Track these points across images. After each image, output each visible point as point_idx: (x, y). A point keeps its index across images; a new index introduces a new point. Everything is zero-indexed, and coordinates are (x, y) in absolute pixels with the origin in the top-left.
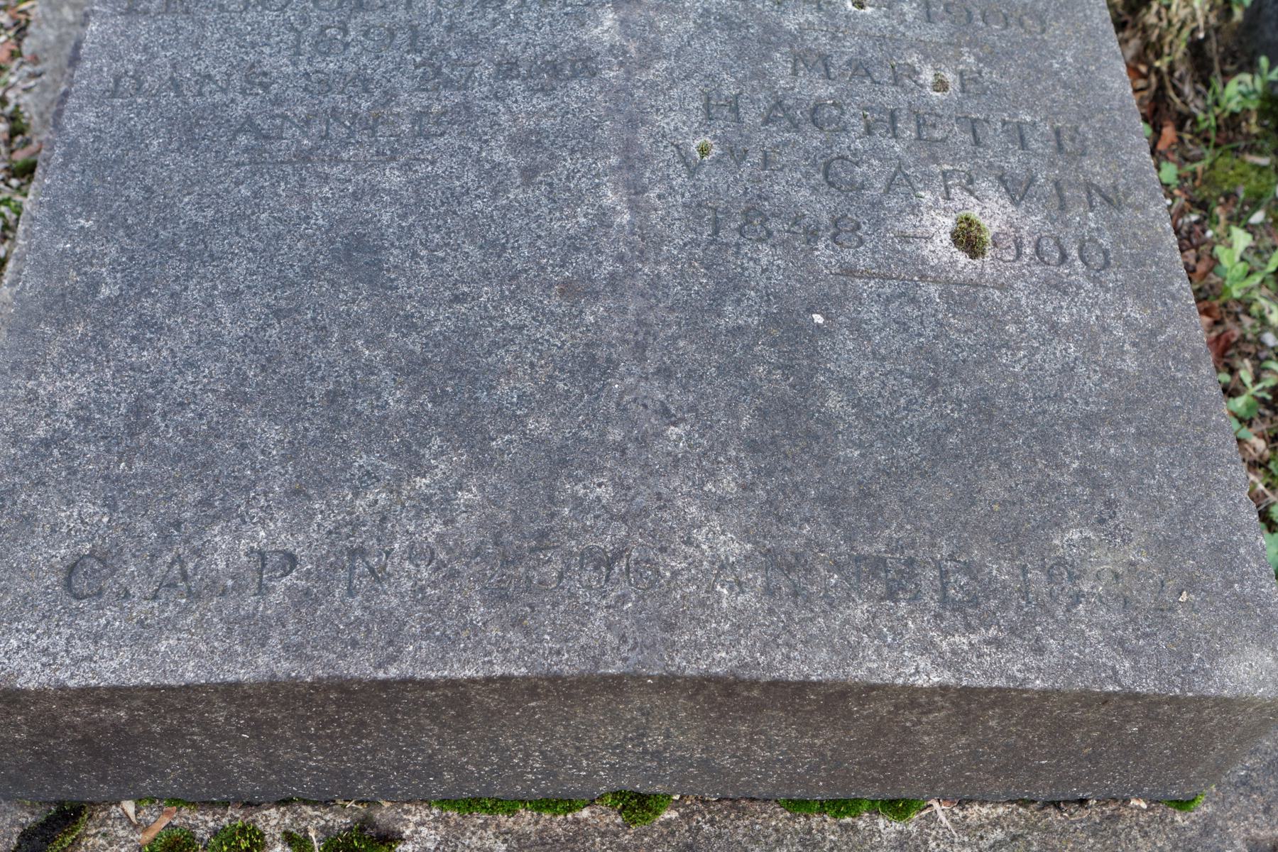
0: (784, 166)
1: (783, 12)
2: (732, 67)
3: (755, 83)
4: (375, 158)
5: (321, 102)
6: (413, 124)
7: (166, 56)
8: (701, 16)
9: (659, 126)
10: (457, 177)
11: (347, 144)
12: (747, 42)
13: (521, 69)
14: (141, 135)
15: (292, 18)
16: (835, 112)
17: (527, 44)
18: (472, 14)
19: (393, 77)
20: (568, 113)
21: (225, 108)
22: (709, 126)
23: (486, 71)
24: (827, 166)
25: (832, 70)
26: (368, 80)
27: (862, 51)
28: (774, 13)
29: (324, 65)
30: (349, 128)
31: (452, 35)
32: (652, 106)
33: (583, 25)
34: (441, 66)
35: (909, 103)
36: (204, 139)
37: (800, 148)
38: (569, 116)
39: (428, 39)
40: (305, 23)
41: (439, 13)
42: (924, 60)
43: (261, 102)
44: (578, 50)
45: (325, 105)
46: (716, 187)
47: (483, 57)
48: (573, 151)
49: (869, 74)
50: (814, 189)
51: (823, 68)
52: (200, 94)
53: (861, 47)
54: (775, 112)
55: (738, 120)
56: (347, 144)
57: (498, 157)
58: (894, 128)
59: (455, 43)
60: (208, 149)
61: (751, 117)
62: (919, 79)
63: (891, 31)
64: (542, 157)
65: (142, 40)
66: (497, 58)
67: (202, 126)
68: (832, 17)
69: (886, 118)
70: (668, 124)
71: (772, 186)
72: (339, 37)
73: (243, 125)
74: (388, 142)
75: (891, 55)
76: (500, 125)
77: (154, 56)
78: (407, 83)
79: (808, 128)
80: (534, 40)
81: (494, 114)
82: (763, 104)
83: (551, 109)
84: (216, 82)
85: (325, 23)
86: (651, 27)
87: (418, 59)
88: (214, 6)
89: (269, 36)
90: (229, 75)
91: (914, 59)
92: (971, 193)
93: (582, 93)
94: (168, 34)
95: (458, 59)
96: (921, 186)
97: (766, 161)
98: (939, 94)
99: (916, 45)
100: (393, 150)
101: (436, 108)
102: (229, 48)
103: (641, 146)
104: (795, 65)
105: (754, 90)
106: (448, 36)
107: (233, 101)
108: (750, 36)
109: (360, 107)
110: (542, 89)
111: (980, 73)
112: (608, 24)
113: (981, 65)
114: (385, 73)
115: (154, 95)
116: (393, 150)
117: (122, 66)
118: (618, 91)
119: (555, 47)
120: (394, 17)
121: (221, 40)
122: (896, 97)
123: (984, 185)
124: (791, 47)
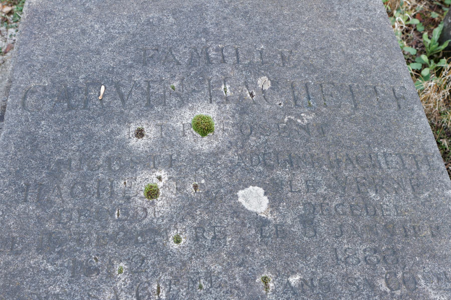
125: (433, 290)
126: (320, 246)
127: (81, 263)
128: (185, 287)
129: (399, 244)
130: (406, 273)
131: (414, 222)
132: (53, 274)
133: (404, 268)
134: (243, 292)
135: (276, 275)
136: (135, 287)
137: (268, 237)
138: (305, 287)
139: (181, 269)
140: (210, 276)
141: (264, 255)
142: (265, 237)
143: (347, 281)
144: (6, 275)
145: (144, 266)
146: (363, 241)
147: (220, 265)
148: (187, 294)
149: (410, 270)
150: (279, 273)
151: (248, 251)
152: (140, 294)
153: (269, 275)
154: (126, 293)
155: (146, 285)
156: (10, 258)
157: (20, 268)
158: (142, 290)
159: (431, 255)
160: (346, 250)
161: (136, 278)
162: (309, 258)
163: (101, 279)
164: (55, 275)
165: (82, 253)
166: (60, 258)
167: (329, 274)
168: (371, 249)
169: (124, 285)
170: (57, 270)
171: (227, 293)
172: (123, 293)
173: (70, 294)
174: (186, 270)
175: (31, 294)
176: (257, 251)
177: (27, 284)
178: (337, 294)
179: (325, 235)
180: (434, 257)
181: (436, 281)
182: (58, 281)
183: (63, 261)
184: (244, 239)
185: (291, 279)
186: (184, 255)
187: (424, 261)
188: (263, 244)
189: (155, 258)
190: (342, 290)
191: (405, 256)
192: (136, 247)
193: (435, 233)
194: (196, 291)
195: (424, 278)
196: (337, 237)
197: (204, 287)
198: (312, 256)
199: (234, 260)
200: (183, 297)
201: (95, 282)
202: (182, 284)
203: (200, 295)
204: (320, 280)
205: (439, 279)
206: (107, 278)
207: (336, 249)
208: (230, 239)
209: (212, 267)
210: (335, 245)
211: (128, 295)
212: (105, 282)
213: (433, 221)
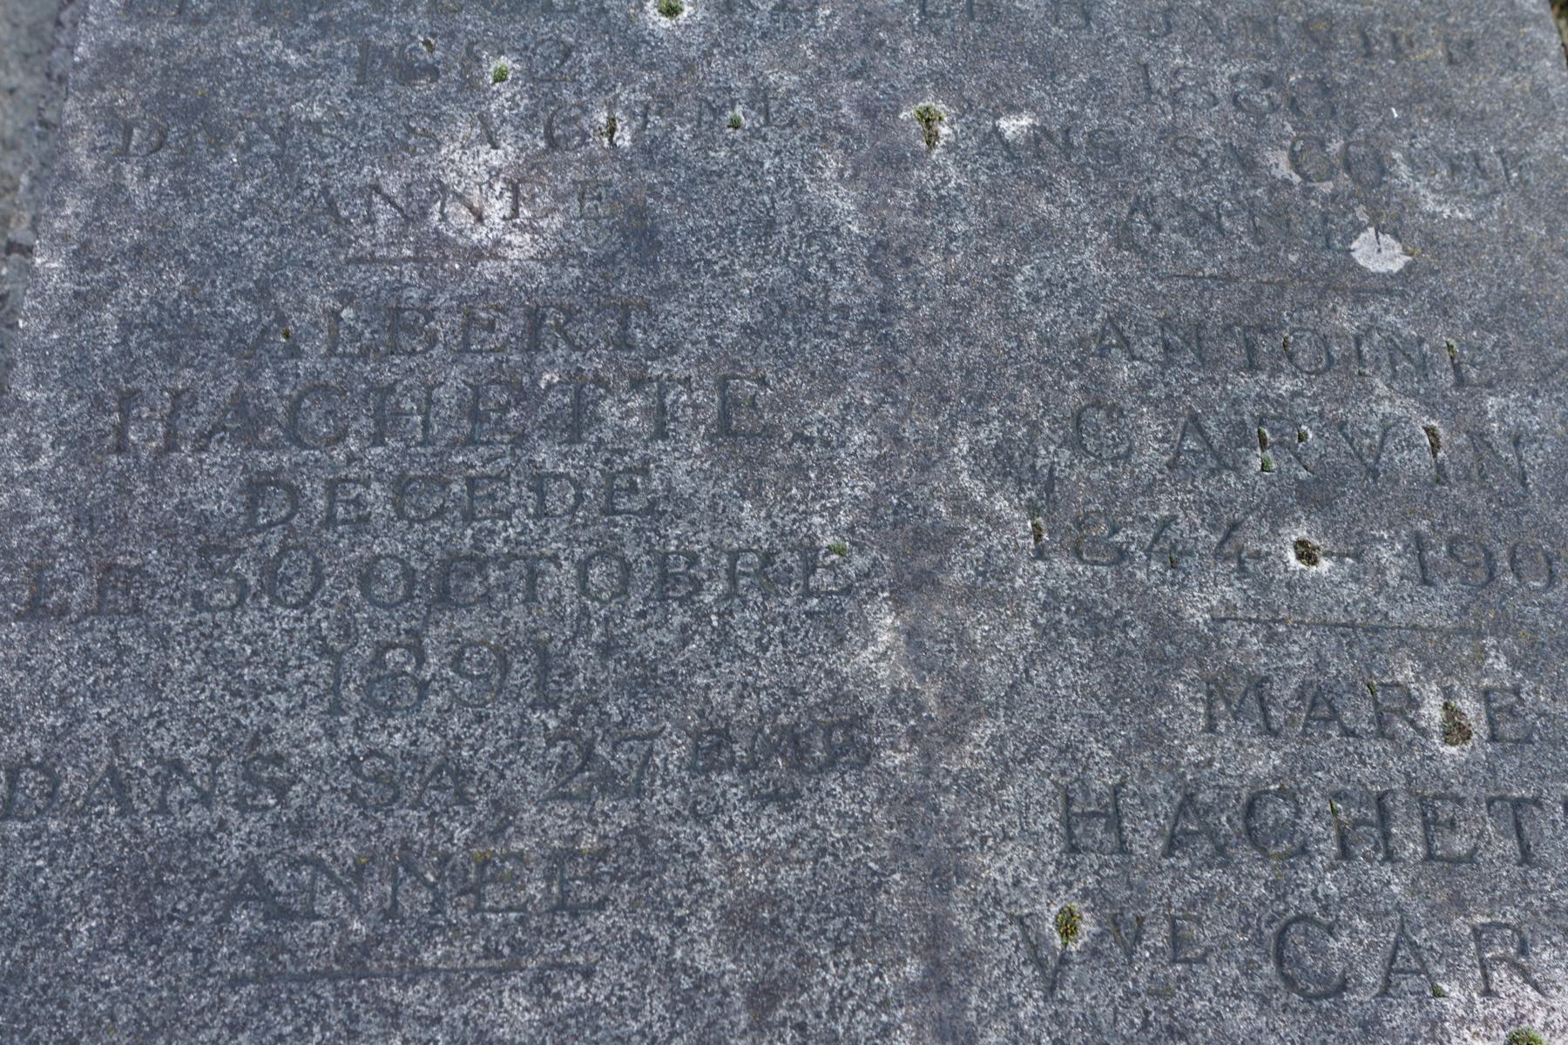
0: (1209, 950)
1: (1183, 586)
2: (1104, 724)
3: (1145, 756)
4: (483, 963)
5: (381, 828)
6: (548, 879)
7: (100, 719)
8: (1045, 606)
9: (988, 879)
10: (632, 1010)
11: (432, 928)
12: (1126, 662)
13: (736, 747)
14: (58, 910)
15: (324, 625)
16: (1285, 812)
17: (745, 685)
18: (642, 615)
19: (507, 766)
20: (823, 851)
21: (208, 843)
22: (1074, 867)
23: (673, 752)
24: (1281, 936)
25: (1273, 713)
26: (463, 774)
27: (1321, 665)
28: (1166, 589)
29: (384, 737)
30: (432, 886)
31: (611, 664)
32: (973, 833)
33: (841, 641)
34: (594, 739)
35: (1407, 775)
36: (171, 919)
37: (1232, 906)
38: (828, 859)
39: (569, 674)
40: (347, 635)
41: (584, 611)
42: (1424, 672)
43: (274, 827)
44: (833, 701)
45: (390, 836)
46: (1094, 1015)
47: (668, 717)
48: (838, 947)
49: (1335, 715)
50: (1264, 1001)
51: (1257, 710)
52: (163, 808)
53: (1318, 654)
54: (1183, 823)
55: (1123, 848)
56: (432, 928)
57: (704, 963)
58: (1387, 836)
59: (616, 684)
60: (180, 944)
61: (1145, 840)
62: (1420, 716)
63: (1365, 611)
64: (784, 961)
65: (55, 680)
66: (693, 721)
67: (166, 885)
68: (1265, 588)
69: (1372, 815)
70: (1002, 871)
71: (1189, 1001)
72: (409, 669)
73: (242, 883)
74: (505, 925)
75: (1369, 668)
76: (704, 882)
77: (77, 718)
78: (536, 781)
79: (1243, 854)
80: (757, 677)
81: (692, 854)
82: (1164, 806)
83: (794, 844)
84: (190, 779)
85: (384, 636)
86: (960, 641)
87: (552, 724)
88: (184, 596)
89: (283, 669)
90: (215, 762)
91: (1406, 673)
92: (1525, 974)
93: (846, 803)
94: (104, 664)
95: (623, 723)
96: (1441, 970)
97: (1177, 940)
98: (1454, 750)
99: (1412, 637)
100: (515, 945)
101: (588, 842)
102: (212, 698)
103: (961, 935)
104: (1210, 706)
105: (1145, 774)
106: (605, 667)
107: (222, 825)
108: (1130, 646)
109: (450, 839)
110: (775, 797)
111: (1516, 691)
112: (885, 637)
113: (1519, 675)
114: (493, 756)
115: (80, 812)
116: (515, 945)
117: (21, 741)
118: (910, 802)
119: (794, 693)
120: (506, 621)
121: (199, 678)
122: (1384, 764)
123: (1545, 956)
124: (1201, 665)
125: (1434, 191)
126: (1098, 54)
127: (385, 53)
128: (691, 120)
129: (1342, 70)
130: (1357, 144)
131: (1397, 23)
132: (303, 74)
133: (1349, 133)
134: (859, 140)
135: (961, 108)
136: (541, 114)
137: (943, 17)
138: (1046, 145)
139: (679, 78)
140: (765, 99)
141: (928, 57)
142: (934, 15)
143: (1175, 145)
144: (165, 70)
145: (571, 68)
146: (1231, 55)
147: (794, 72)
148: (695, 137)
149: (1367, 136)
150: (970, 106)
151: (881, 43)
152: (558, 132)
153: (940, 107)
154: (517, 128)
155: (575, 112)
156: (177, 30)
157: (206, 57)
158: (564, 122)
159: (1437, 108)
160: (1176, 73)
161: (545, 94)
162: (1064, 78)
163: (444, 92)
164: (307, 78)
165: (387, 28)
166: (324, 36)
167: (1119, 123)
168: (1254, 77)
169: (511, 109)
170: (315, 66)
171: (812, 140)
172: (508, 128)
173: (353, 123)
174: (694, 81)
175: (241, 118)
176: (908, 46)
177: (228, 95)
178: (1141, 172)
179: (1117, 29)
180: (1447, 114)
181: (1445, 173)
182: (318, 91)
183: (331, 46)
184: (869, 14)
185: (1003, 124)
186: (690, 45)
187: (1415, 119)
188: (925, 30)
189: (603, 48)
190: (1156, 164)
191: (1357, 101)
192: (547, 21)
193: (1457, 55)
194: (721, 132)
195: (1410, 161)
196: (1154, 38)
197: (746, 123)
198: (1070, 77)
199: (835, 61)
200: (684, 144)
201: (427, 99)
202: (680, 114)
203: (734, 141)
204: (1090, 135)
205: (1454, 169)
206: (460, 90)
207: (1146, 66)
208: (828, 12)
209: (772, 78)
210: (1146, 55)
211: (521, 132)
212: (455, 100)
213: (1455, 25)
